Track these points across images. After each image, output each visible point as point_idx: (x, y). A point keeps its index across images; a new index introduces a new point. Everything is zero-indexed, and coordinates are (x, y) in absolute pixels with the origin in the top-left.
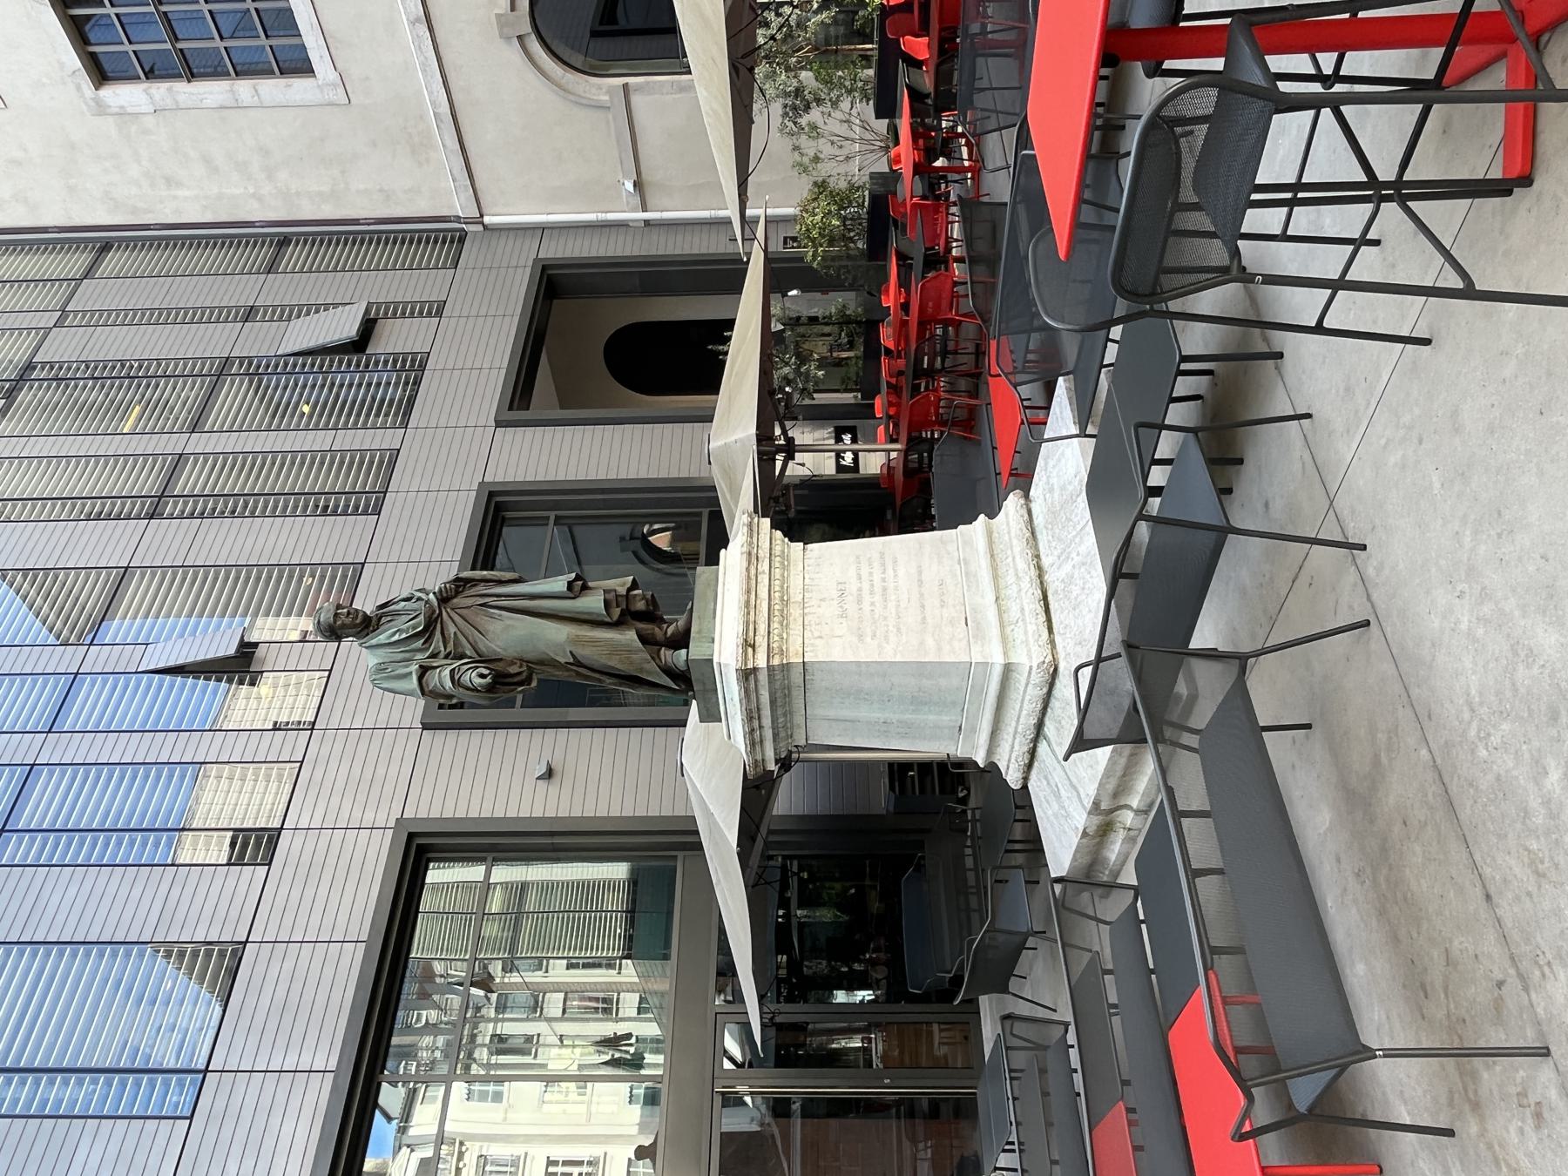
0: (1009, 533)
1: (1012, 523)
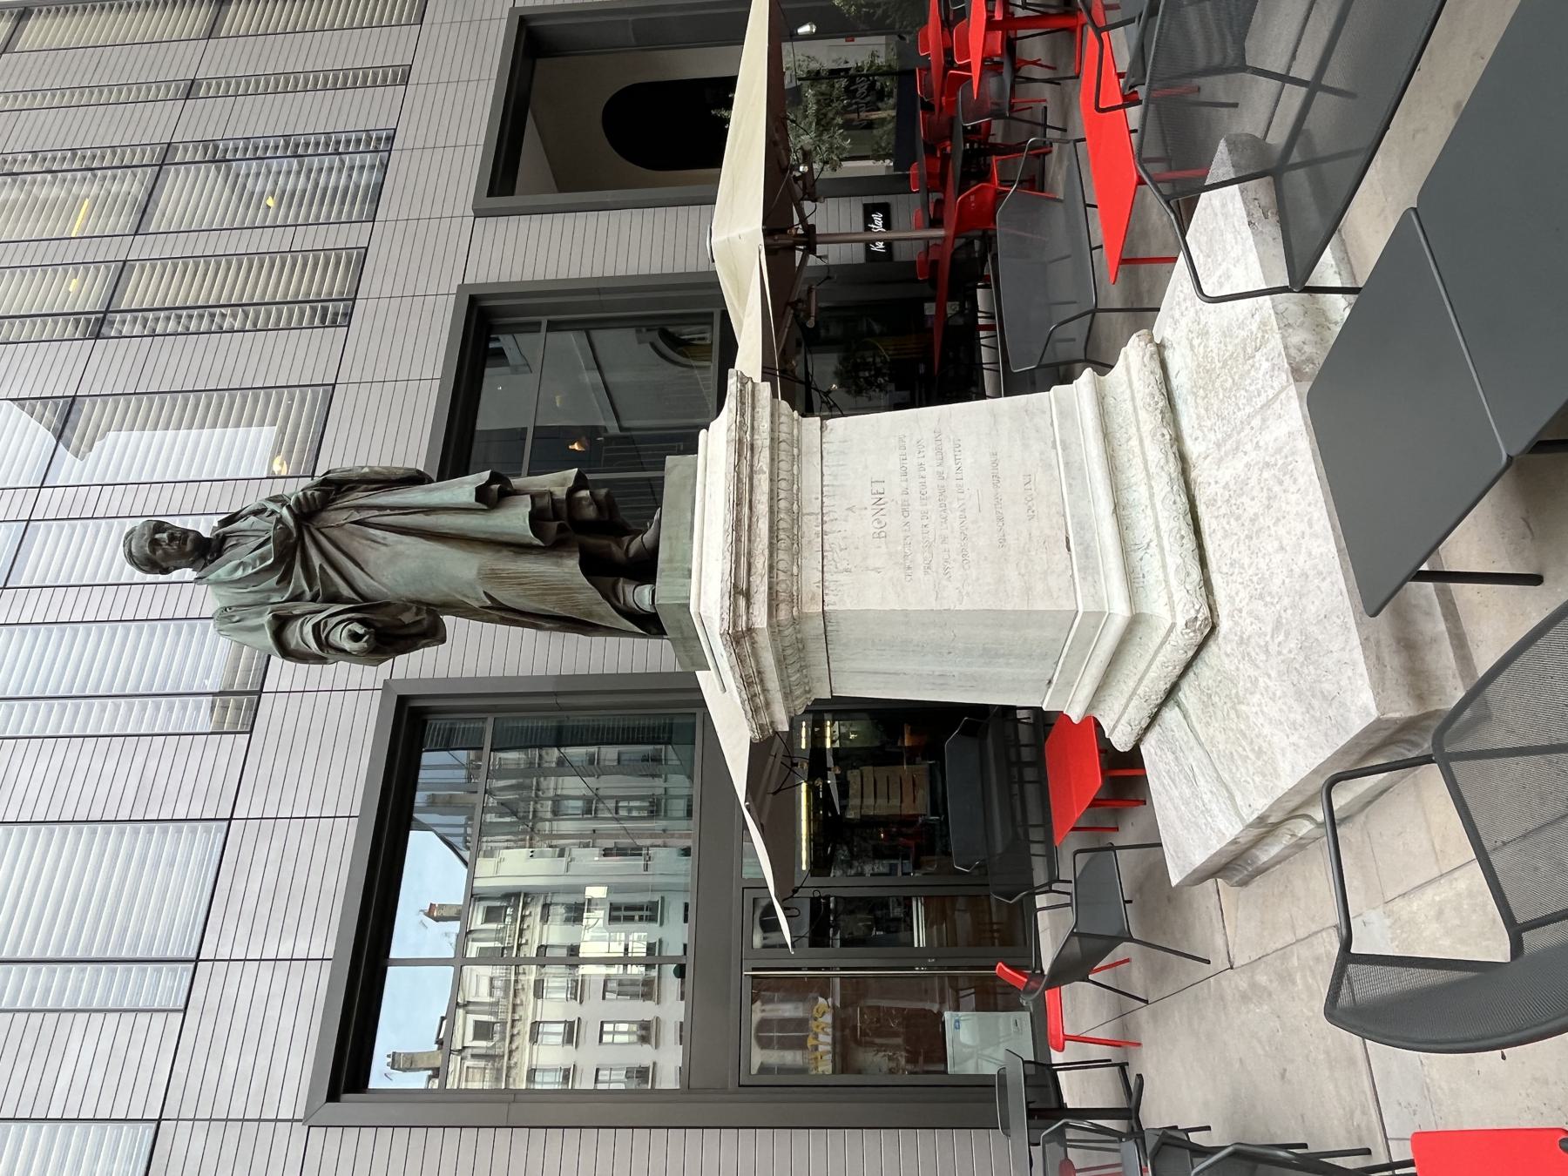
0: (1133, 399)
1: (1137, 384)
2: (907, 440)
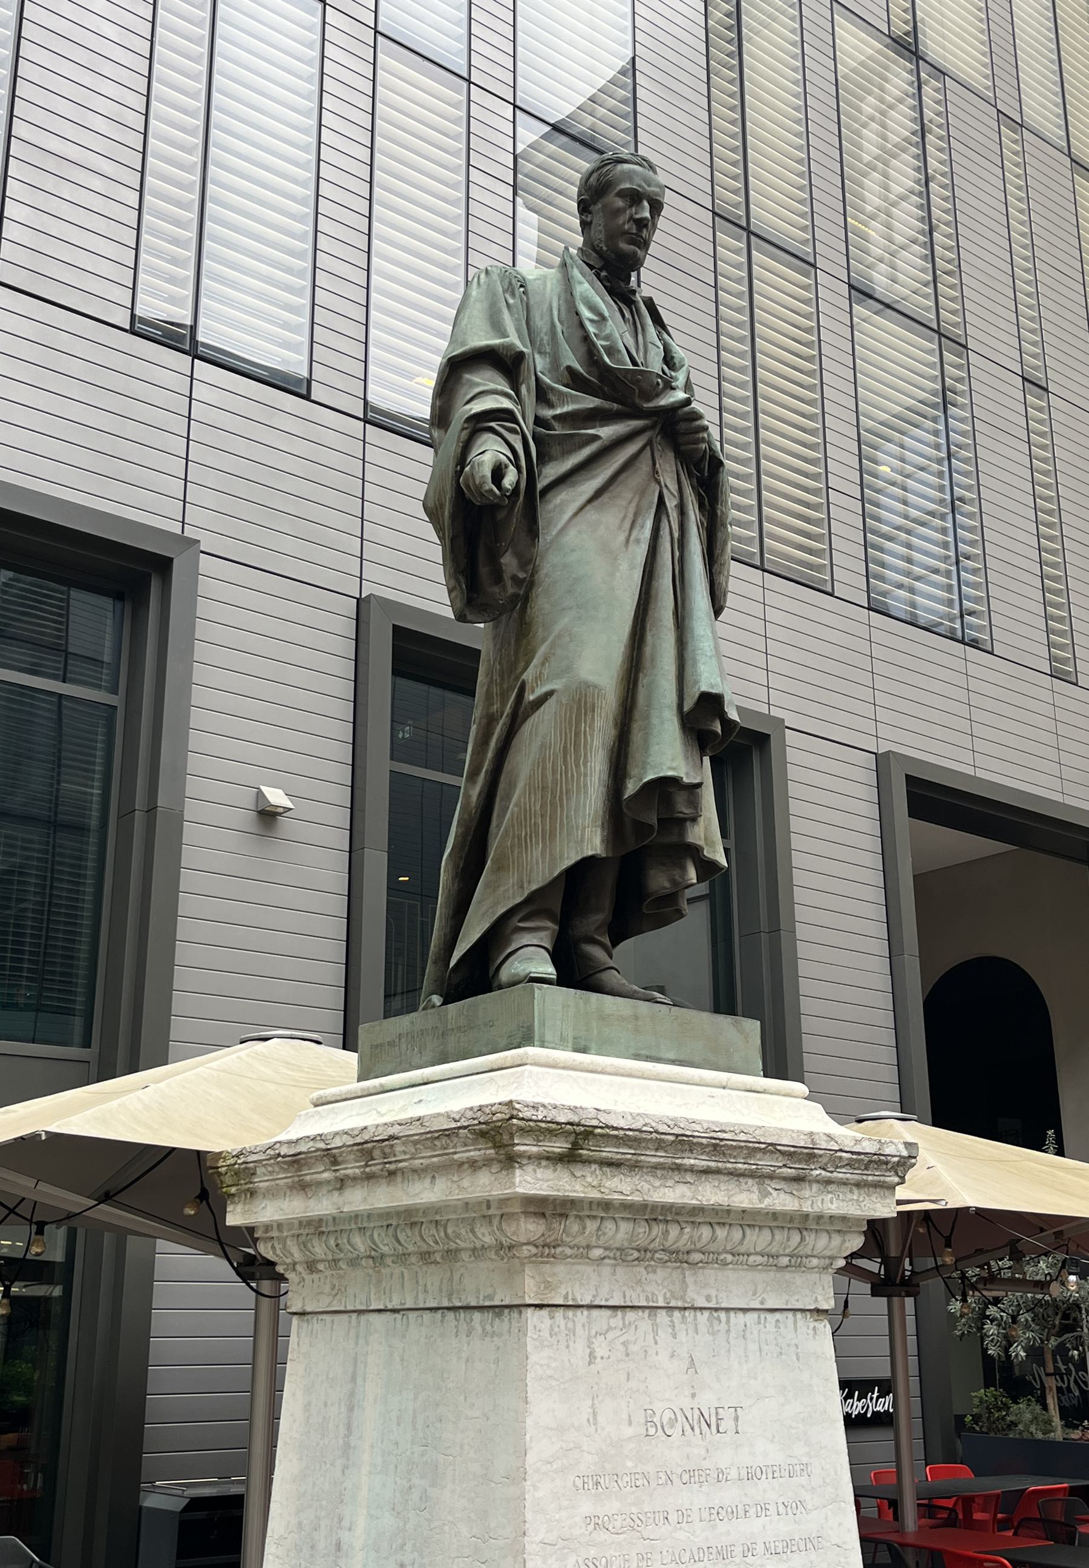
2: (803, 1480)
